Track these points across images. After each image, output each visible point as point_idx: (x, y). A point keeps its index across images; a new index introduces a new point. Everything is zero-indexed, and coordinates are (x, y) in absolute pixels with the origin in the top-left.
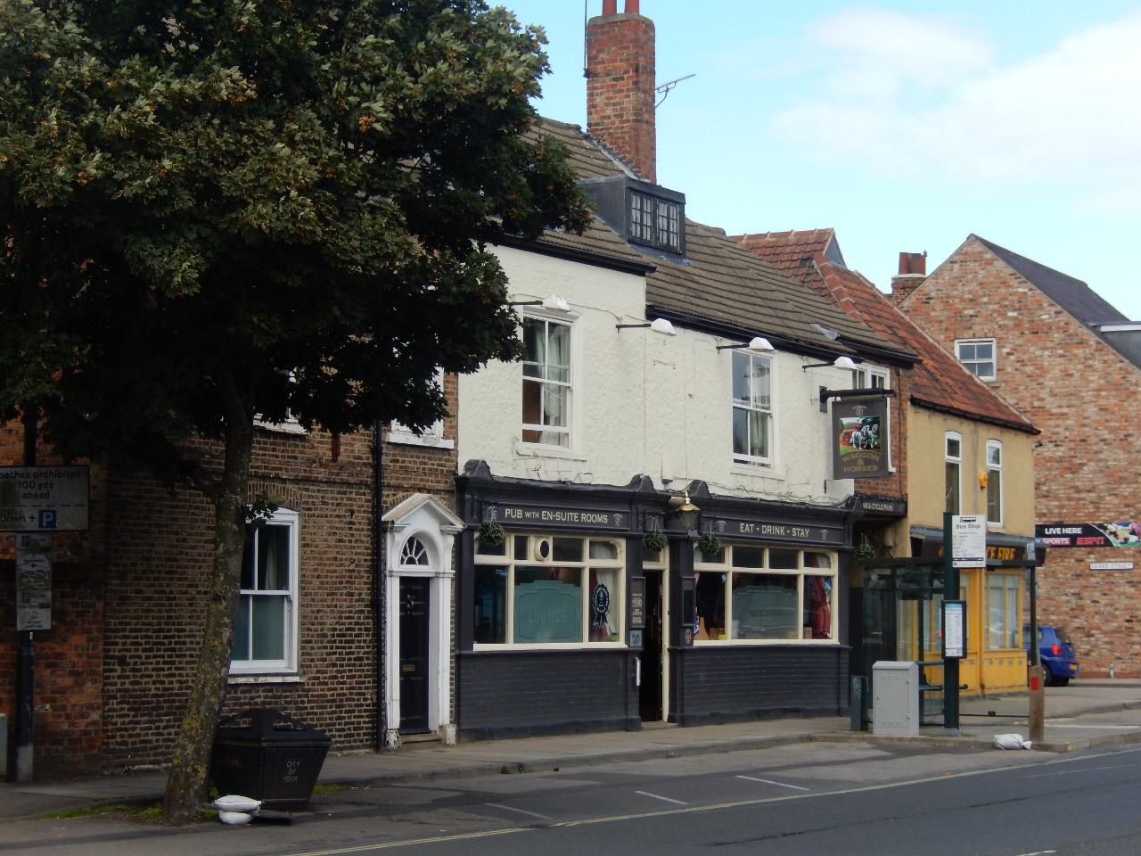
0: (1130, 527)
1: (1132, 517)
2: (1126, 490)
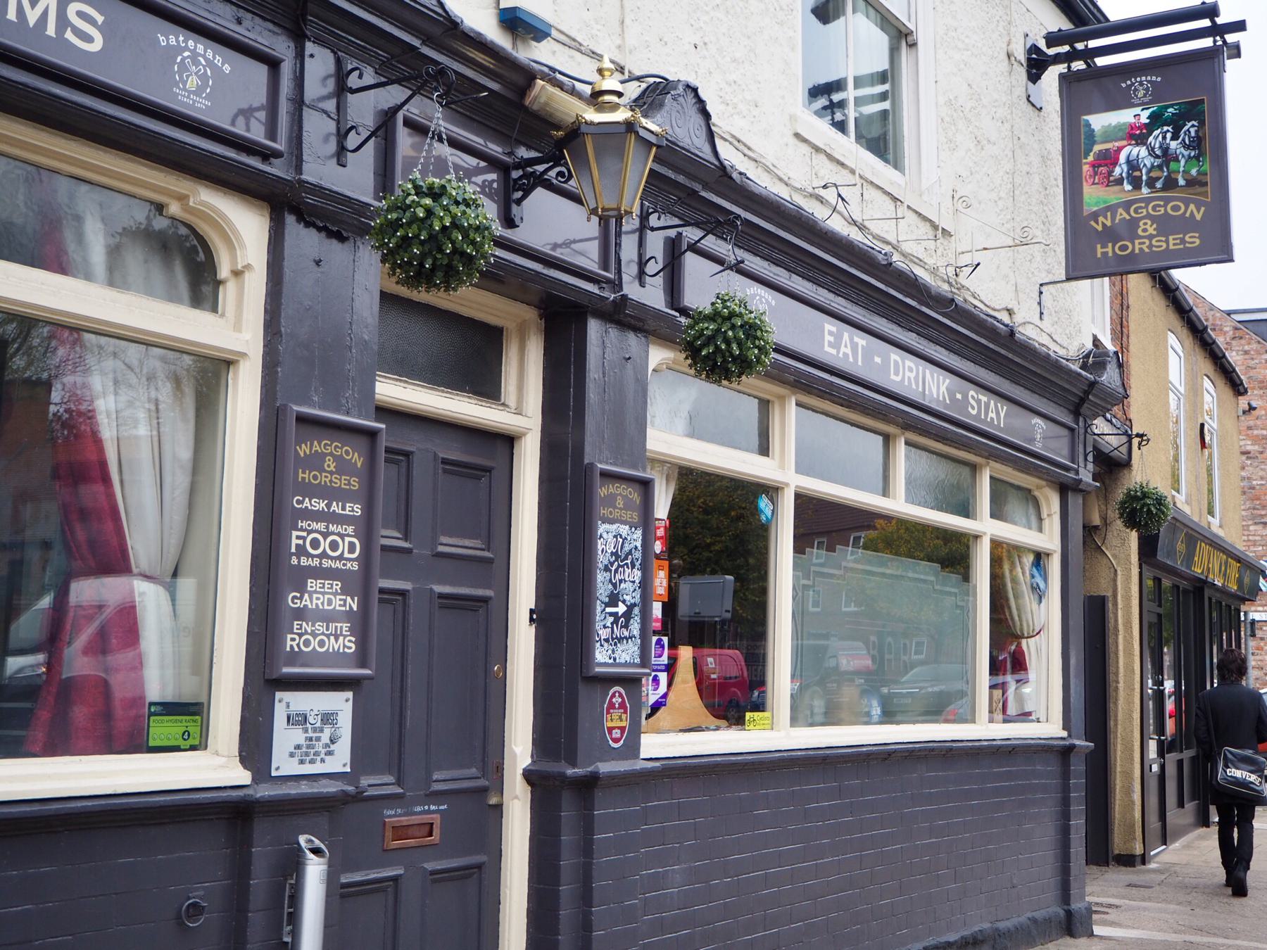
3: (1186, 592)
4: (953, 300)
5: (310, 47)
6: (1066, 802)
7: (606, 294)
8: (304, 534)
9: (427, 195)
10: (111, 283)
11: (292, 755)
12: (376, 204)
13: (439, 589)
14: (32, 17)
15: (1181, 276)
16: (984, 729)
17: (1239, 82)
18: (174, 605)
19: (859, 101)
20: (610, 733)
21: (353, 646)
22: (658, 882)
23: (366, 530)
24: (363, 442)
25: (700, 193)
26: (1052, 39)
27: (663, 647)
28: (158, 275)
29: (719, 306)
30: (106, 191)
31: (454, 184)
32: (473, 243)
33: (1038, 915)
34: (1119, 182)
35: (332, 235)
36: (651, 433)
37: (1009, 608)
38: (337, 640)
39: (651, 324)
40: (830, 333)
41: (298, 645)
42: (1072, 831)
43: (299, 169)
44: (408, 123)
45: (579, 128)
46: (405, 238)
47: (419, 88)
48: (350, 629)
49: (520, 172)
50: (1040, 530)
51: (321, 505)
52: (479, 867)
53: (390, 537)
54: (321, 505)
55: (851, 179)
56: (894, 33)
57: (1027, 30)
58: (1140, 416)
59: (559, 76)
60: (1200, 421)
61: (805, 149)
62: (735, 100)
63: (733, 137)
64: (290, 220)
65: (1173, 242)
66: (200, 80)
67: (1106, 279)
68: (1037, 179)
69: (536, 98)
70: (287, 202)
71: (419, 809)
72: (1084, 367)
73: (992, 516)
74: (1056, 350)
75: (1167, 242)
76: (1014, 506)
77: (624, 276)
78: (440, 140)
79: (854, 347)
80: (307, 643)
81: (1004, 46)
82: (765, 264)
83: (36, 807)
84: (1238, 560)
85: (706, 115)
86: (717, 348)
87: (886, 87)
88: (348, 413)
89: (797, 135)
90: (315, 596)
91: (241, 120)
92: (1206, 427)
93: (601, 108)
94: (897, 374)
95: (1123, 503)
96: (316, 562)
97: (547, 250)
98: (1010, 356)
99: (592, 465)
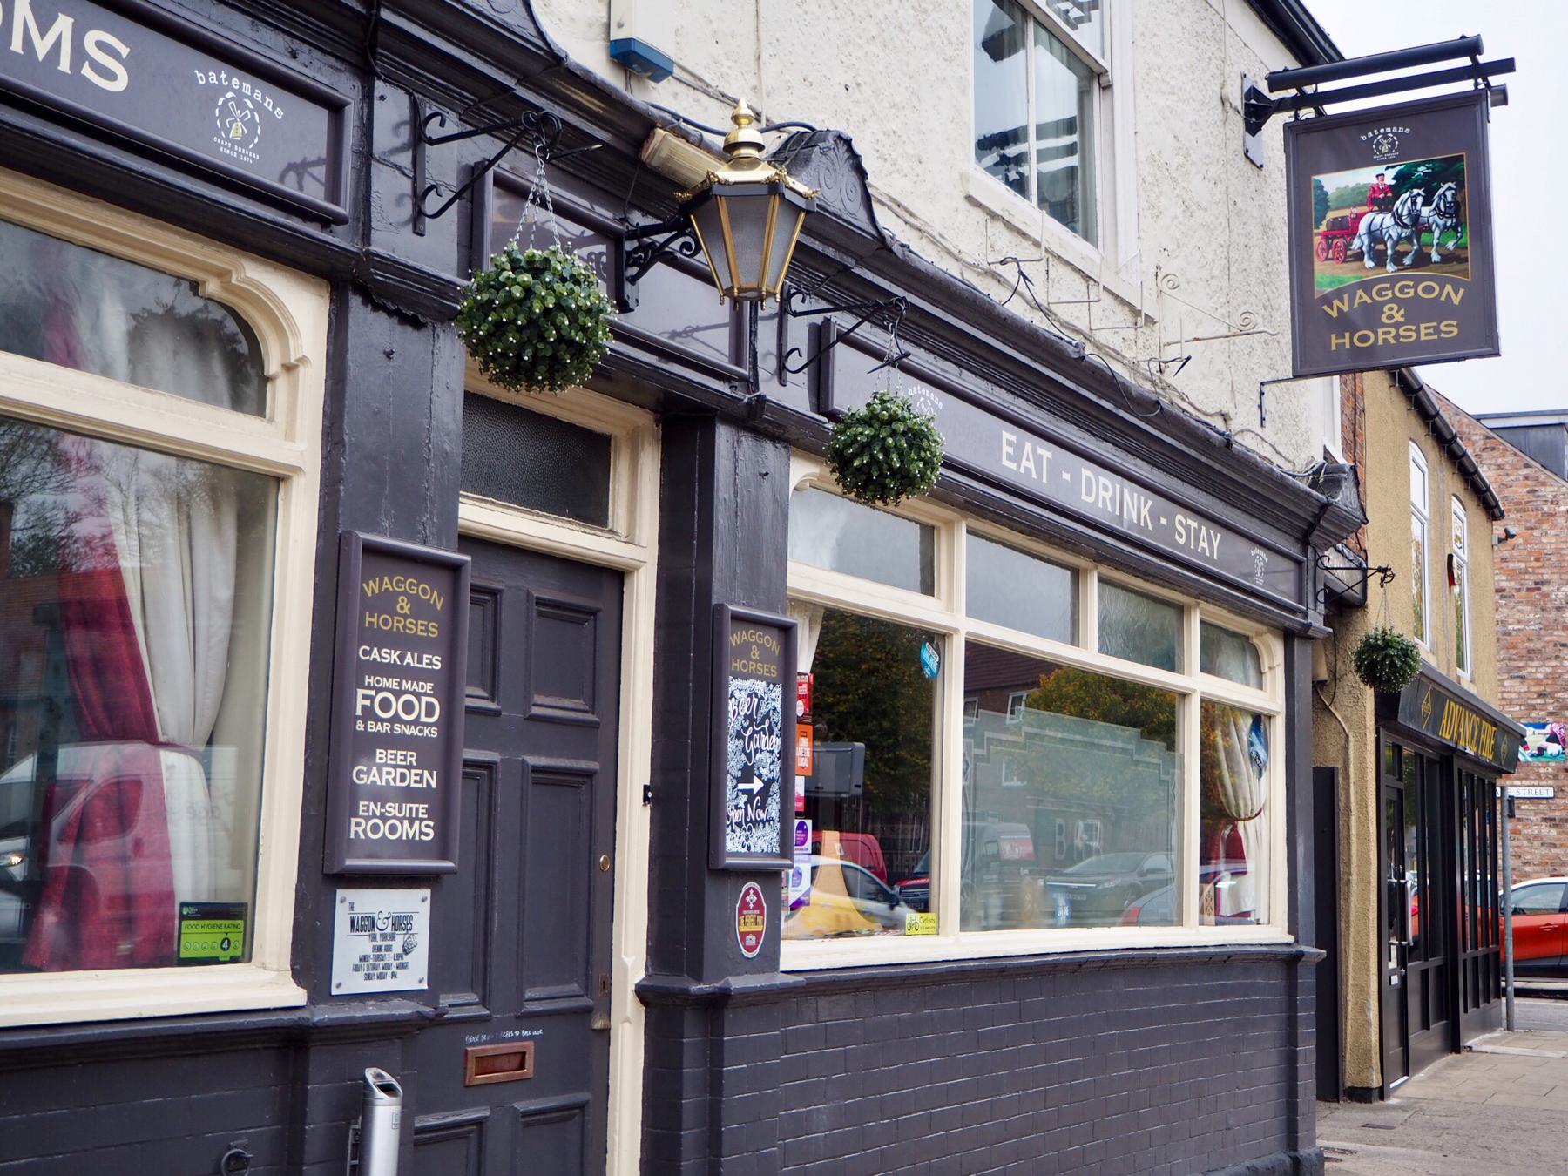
0: (1548, 730)
1: (1551, 714)
2: (1539, 670)
3: (1430, 761)
4: (1158, 402)
5: (380, 87)
6: (1292, 1023)
7: (738, 395)
8: (372, 693)
9: (526, 271)
10: (134, 380)
11: (356, 968)
12: (465, 283)
13: (533, 760)
14: (42, 48)
15: (1430, 376)
16: (1194, 933)
17: (1506, 134)
18: (208, 779)
19: (1043, 155)
20: (743, 940)
21: (431, 832)
22: (801, 1124)
23: (448, 689)
24: (444, 578)
25: (855, 270)
26: (1276, 81)
27: (806, 831)
28: (190, 368)
29: (878, 407)
30: (126, 266)
31: (560, 257)
32: (584, 329)
33: (1260, 1163)
34: (1359, 256)
35: (405, 320)
36: (792, 566)
37: (1223, 785)
38: (411, 825)
39: (793, 432)
40: (1009, 443)
41: (364, 831)
42: (1300, 1058)
43: (366, 238)
44: (499, 182)
45: (710, 189)
46: (498, 324)
47: (517, 139)
48: (428, 811)
49: (635, 244)
50: (1260, 686)
51: (391, 656)
52: (582, 1106)
53: (474, 696)
54: (391, 656)
55: (1035, 253)
56: (1084, 72)
57: (1244, 69)
58: (1377, 544)
59: (684, 125)
60: (1448, 552)
61: (979, 215)
62: (894, 155)
63: (893, 200)
64: (355, 301)
65: (1425, 332)
66: (247, 126)
67: (1336, 378)
68: (1256, 254)
69: (655, 151)
70: (351, 280)
71: (508, 1035)
72: (1314, 485)
73: (1100, 651)
74: (1280, 465)
75: (1418, 331)
76: (1229, 657)
77: (760, 372)
78: (543, 205)
79: (1038, 460)
80: (375, 828)
81: (1217, 88)
82: (930, 357)
83: (43, 1035)
84: (1494, 723)
85: (861, 173)
86: (873, 457)
87: (1074, 138)
88: (425, 542)
89: (969, 198)
90: (385, 770)
91: (292, 176)
92: (1455, 559)
93: (736, 163)
94: (1089, 493)
95: (1360, 653)
96: (386, 728)
97: (664, 339)
98: (1226, 471)
99: (721, 607)
